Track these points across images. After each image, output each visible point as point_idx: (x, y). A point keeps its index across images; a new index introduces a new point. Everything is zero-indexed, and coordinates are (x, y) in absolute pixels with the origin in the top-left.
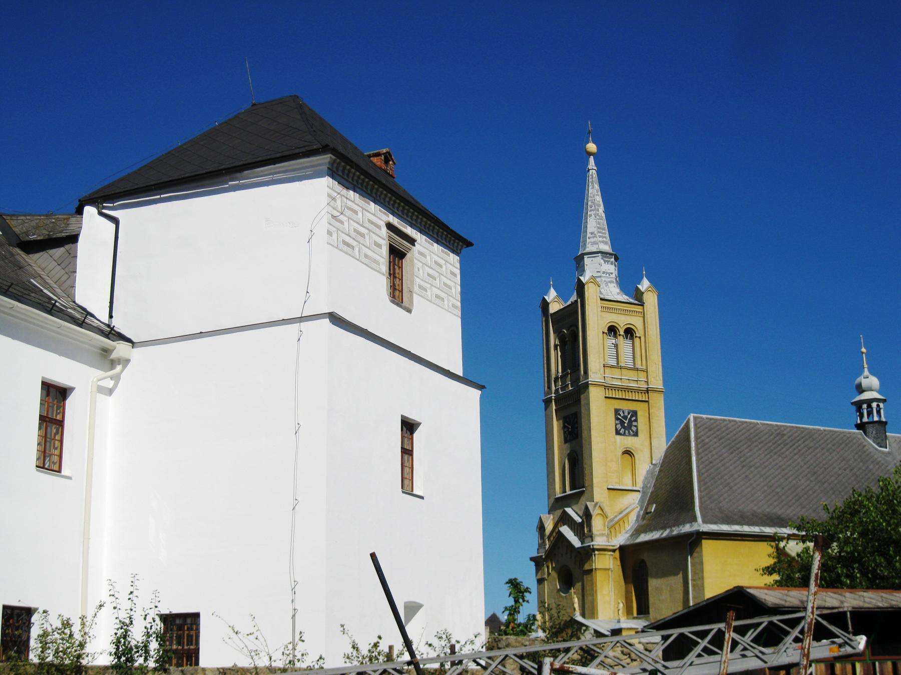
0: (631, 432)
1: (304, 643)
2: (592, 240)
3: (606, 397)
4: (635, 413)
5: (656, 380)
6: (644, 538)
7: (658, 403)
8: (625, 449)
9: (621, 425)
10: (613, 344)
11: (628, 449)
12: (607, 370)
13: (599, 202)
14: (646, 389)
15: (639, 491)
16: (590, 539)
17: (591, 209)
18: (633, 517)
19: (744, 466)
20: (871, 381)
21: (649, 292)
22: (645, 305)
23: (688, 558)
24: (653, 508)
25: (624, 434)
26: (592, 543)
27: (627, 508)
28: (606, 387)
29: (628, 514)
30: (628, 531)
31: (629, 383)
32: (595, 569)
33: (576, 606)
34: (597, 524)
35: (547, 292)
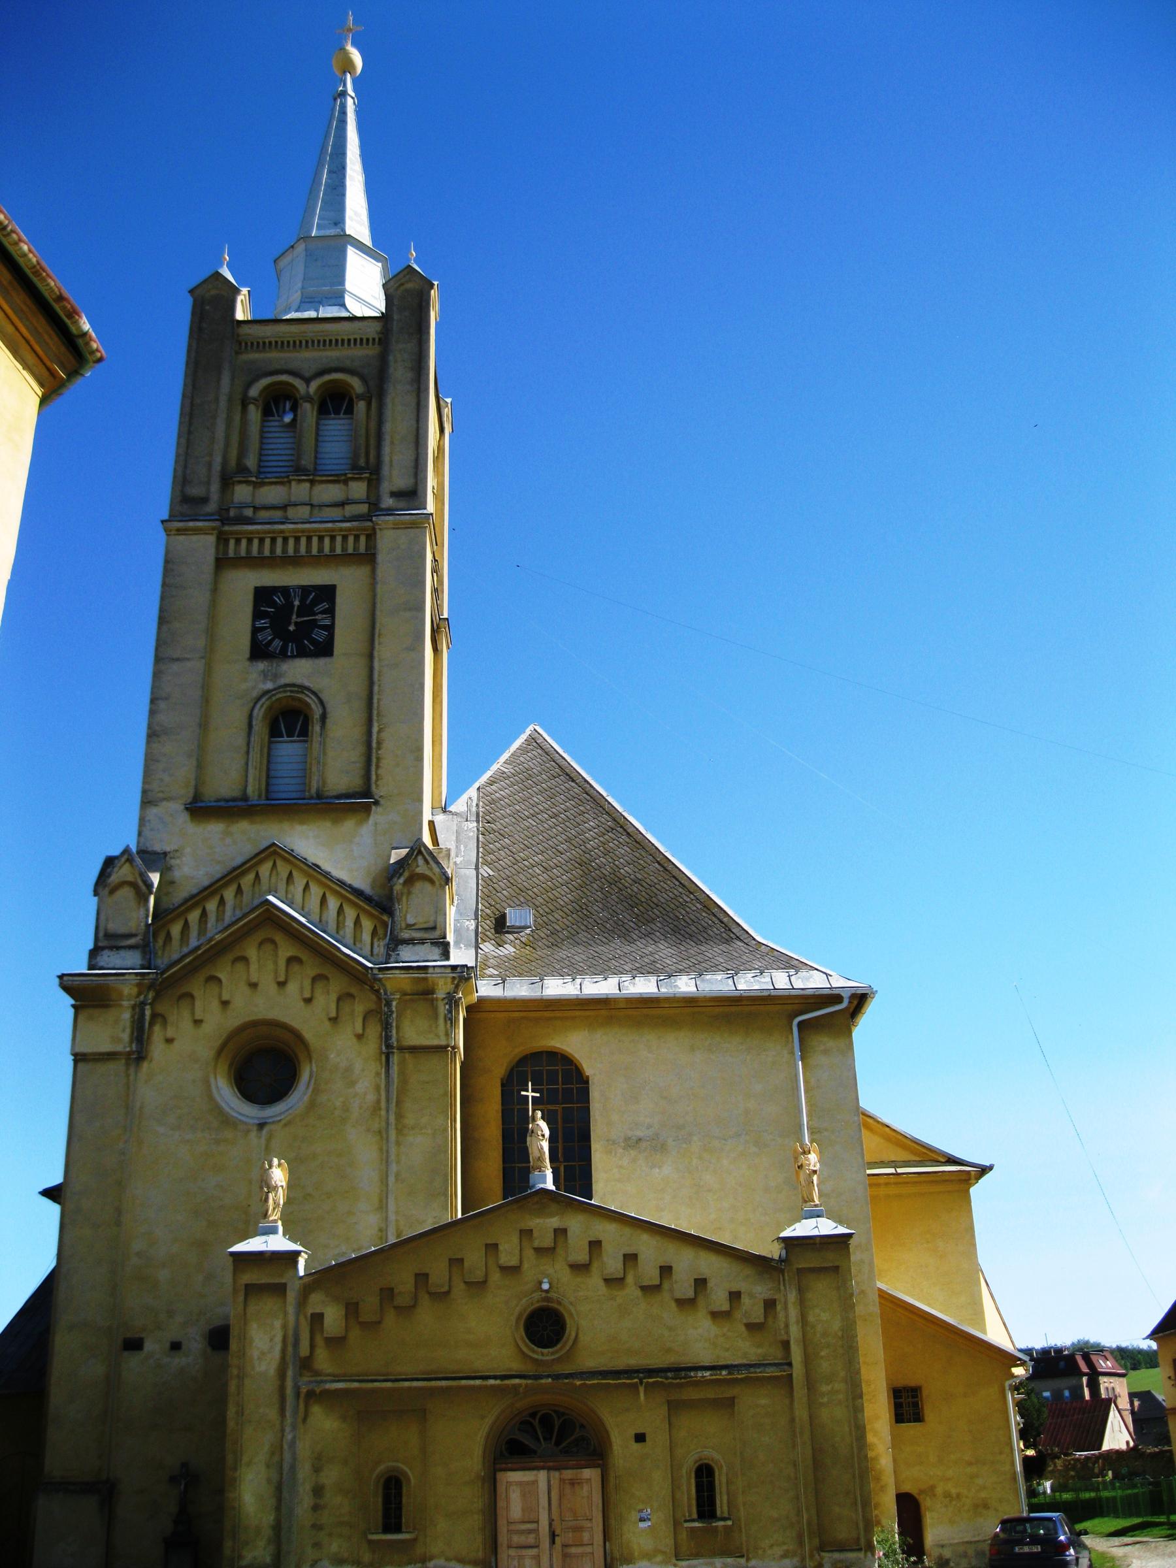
6: (556, 987)
16: (436, 952)
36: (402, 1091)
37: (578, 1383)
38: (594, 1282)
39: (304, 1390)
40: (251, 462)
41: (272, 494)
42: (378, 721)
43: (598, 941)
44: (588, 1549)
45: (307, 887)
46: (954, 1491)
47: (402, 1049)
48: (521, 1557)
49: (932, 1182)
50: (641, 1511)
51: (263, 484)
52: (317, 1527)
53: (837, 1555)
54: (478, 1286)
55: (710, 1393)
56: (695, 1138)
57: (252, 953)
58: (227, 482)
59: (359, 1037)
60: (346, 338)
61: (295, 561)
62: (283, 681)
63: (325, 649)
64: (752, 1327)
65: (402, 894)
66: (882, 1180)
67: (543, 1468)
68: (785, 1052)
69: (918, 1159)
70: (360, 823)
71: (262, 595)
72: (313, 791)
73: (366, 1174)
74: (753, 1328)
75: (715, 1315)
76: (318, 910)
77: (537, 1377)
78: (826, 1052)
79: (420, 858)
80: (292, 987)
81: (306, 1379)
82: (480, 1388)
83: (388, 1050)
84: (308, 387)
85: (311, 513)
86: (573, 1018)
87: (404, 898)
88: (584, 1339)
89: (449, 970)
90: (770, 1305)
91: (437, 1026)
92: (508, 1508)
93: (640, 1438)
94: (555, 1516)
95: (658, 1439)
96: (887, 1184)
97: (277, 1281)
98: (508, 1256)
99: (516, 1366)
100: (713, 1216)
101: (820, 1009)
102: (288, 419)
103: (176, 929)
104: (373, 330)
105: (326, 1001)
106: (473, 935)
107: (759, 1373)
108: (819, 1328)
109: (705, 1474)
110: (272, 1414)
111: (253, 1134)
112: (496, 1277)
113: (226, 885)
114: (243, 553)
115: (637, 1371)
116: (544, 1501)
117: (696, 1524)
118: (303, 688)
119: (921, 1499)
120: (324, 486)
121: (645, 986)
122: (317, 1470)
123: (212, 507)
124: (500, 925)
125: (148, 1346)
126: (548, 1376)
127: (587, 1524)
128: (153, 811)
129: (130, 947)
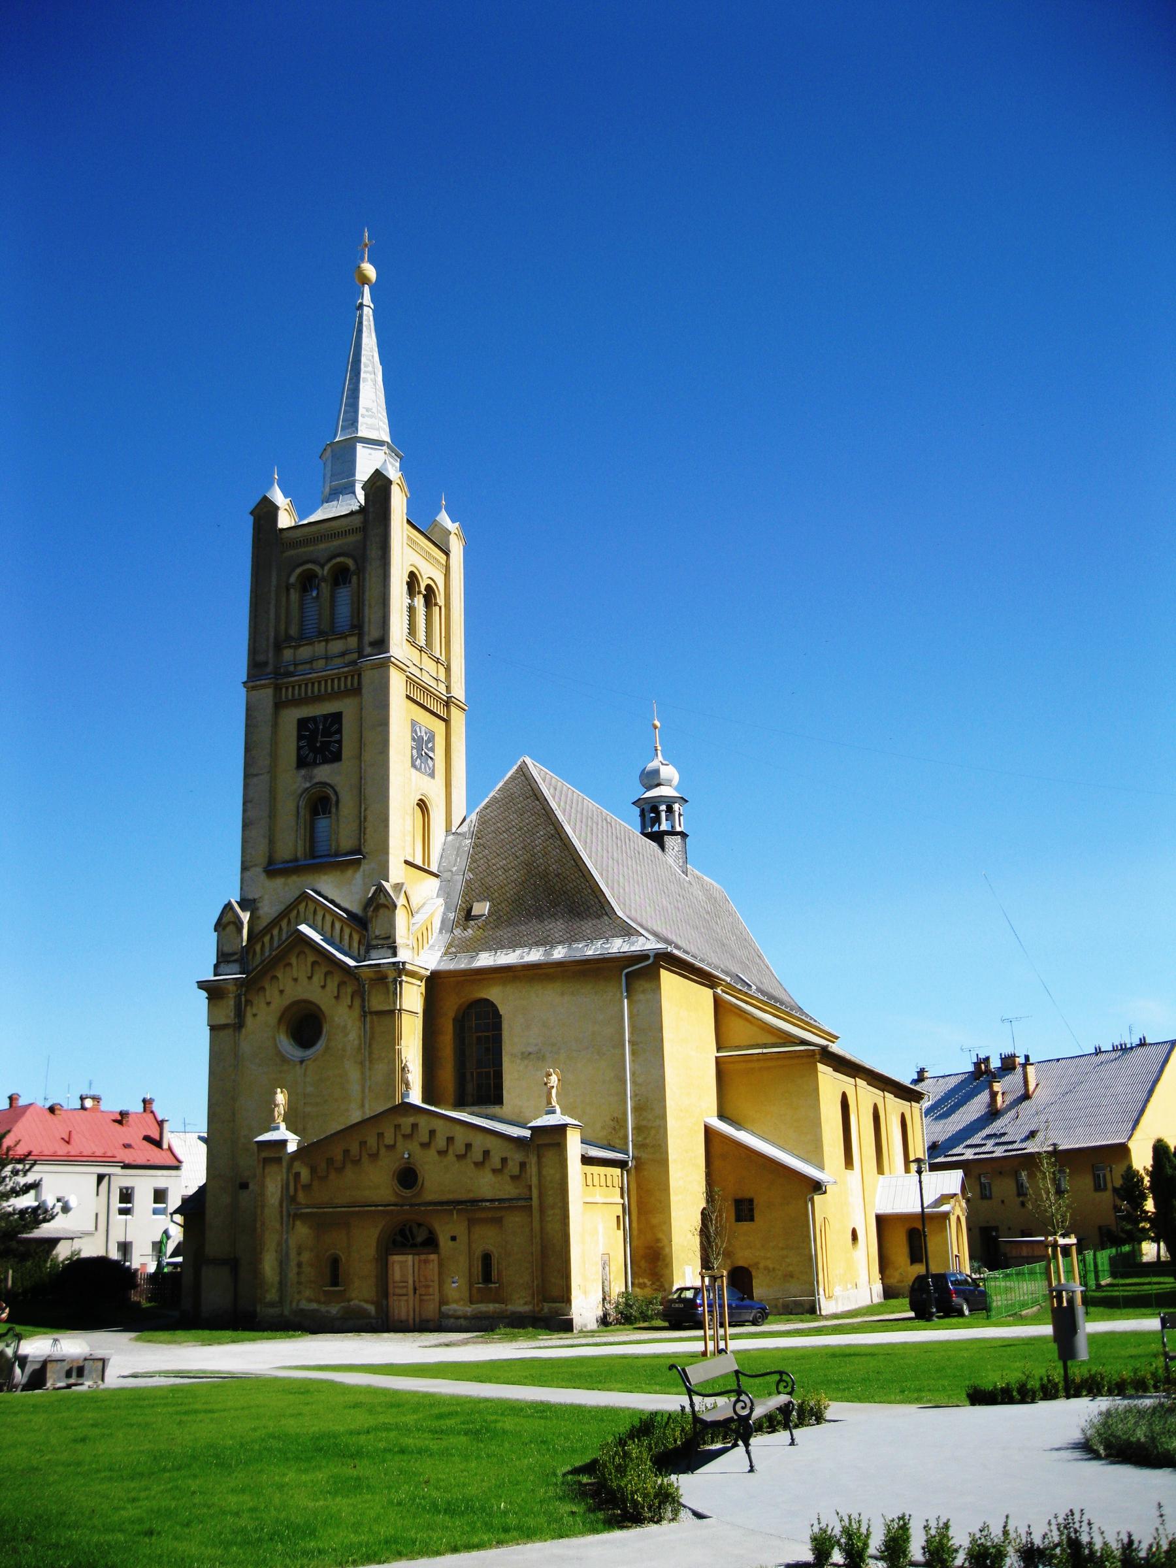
6: (485, 960)
11: (423, 798)
14: (445, 698)
16: (390, 952)
20: (668, 772)
22: (451, 555)
24: (482, 908)
36: (372, 1038)
37: (423, 1208)
38: (432, 1153)
39: (292, 1213)
40: (293, 631)
41: (305, 652)
42: (365, 803)
43: (522, 922)
44: (432, 1297)
45: (324, 916)
46: (771, 1266)
47: (371, 1013)
48: (400, 1300)
50: (453, 1278)
51: (300, 646)
52: (299, 1283)
53: (551, 1304)
54: (374, 1157)
55: (490, 1215)
56: (563, 1051)
57: (294, 961)
58: (278, 648)
59: (350, 1007)
60: (340, 531)
61: (318, 699)
63: (337, 757)
64: (514, 1178)
65: (372, 918)
66: (755, 1058)
67: (411, 1254)
68: (618, 992)
70: (355, 872)
71: (302, 723)
72: (333, 851)
73: (355, 1088)
74: (514, 1178)
75: (494, 1171)
76: (330, 930)
77: (402, 1206)
78: (643, 992)
79: (381, 894)
80: (315, 978)
81: (293, 1207)
82: (375, 1211)
83: (365, 1013)
84: (323, 570)
85: (326, 663)
86: (493, 978)
87: (374, 920)
88: (427, 1184)
89: (391, 965)
90: (523, 1165)
91: (389, 998)
92: (393, 1275)
93: (454, 1238)
94: (416, 1279)
95: (463, 1238)
97: (277, 1156)
98: (389, 1139)
99: (393, 1199)
100: (571, 1100)
102: (314, 594)
103: (258, 948)
105: (332, 986)
106: (451, 922)
107: (515, 1203)
108: (548, 1178)
109: (487, 1258)
110: (278, 1226)
111: (298, 1067)
112: (383, 1151)
113: (282, 919)
114: (290, 697)
115: (453, 1202)
116: (411, 1271)
117: (480, 1285)
118: (325, 784)
119: (750, 1269)
120: (334, 642)
121: (535, 956)
122: (299, 1254)
123: (270, 668)
124: (468, 916)
125: (251, 1186)
126: (407, 1205)
127: (431, 1284)
128: (248, 874)
129: (235, 961)
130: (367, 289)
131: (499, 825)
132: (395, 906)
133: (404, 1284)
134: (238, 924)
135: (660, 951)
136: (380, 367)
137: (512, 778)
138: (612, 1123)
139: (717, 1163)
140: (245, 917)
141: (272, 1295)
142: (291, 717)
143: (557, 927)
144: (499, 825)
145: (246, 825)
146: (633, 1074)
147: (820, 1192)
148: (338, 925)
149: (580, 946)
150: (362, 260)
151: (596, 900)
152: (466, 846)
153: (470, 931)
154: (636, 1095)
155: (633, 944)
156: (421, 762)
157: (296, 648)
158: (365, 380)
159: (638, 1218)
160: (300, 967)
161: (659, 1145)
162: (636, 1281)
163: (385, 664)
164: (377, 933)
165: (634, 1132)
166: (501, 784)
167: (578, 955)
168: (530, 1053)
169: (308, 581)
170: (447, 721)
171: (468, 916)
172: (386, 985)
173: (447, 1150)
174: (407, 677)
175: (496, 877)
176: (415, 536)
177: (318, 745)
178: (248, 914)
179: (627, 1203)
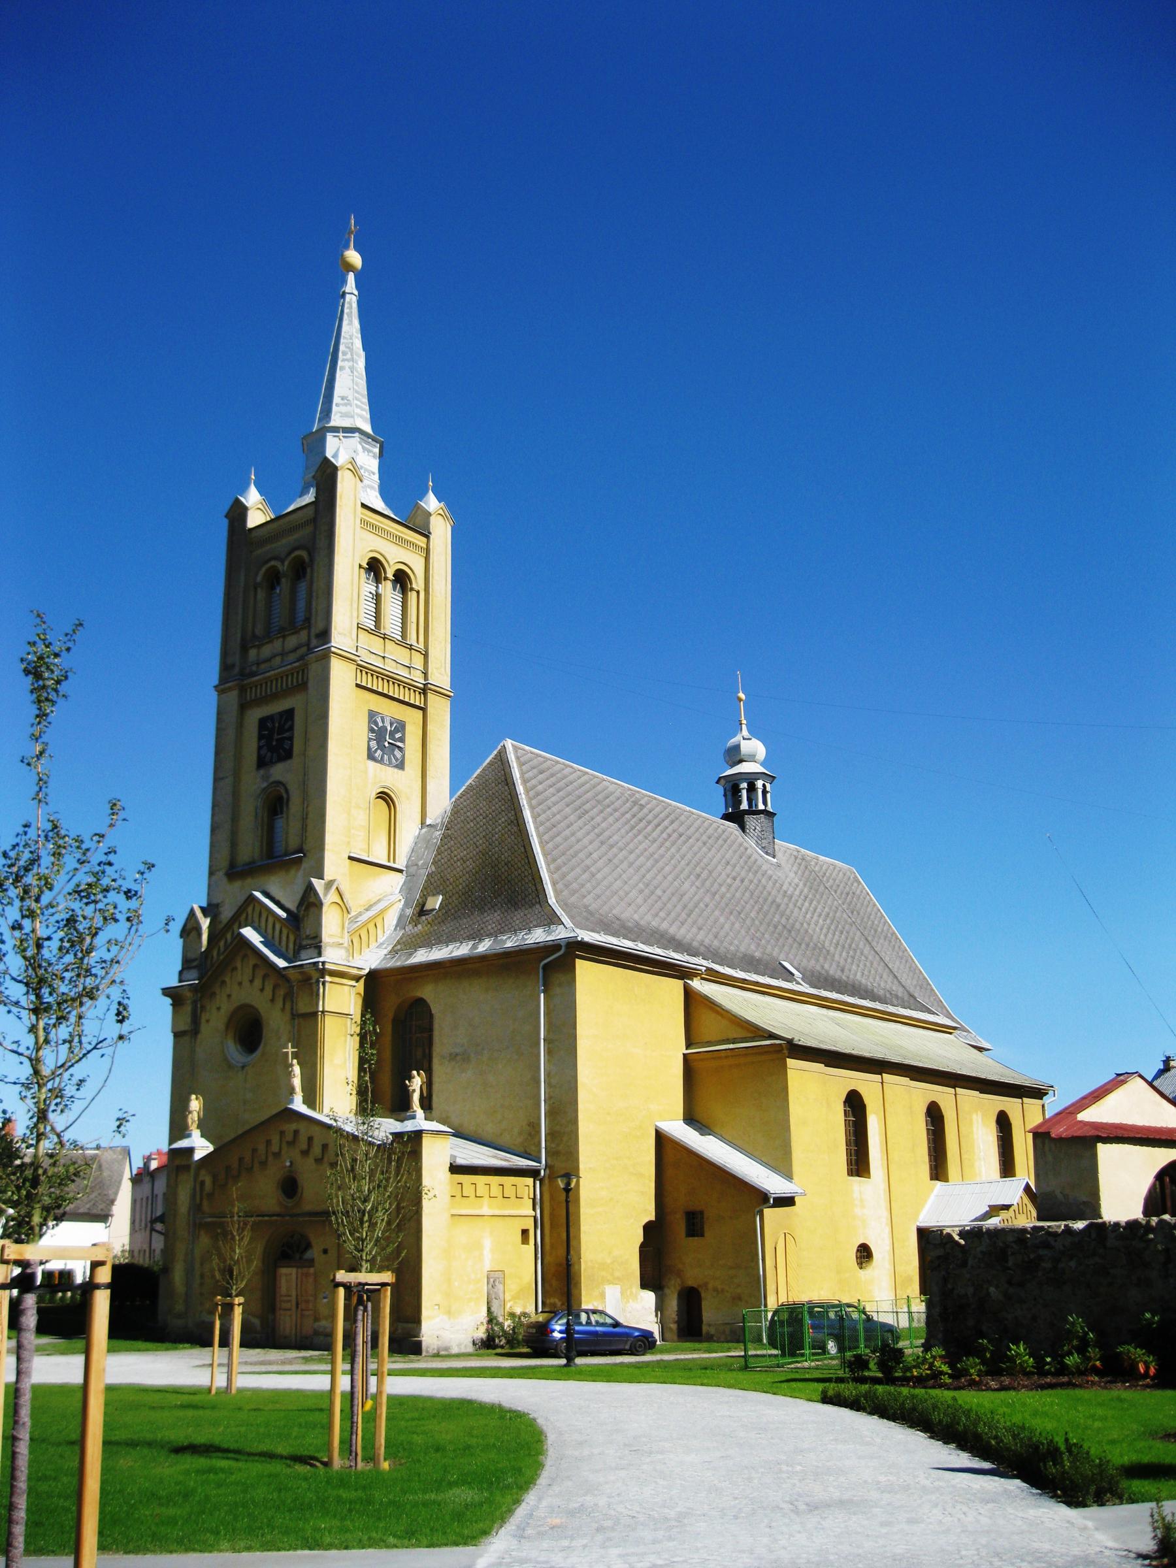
0: (394, 760)
1: (107, 953)
2: (343, 409)
3: (358, 686)
4: (401, 726)
5: (440, 674)
6: (422, 956)
7: (440, 711)
8: (382, 790)
9: (378, 743)
10: (371, 593)
11: (386, 790)
12: (362, 634)
13: (358, 348)
14: (422, 686)
15: (400, 871)
17: (345, 357)
18: (392, 918)
19: (602, 843)
20: (754, 747)
21: (439, 517)
22: (432, 537)
23: (539, 997)
24: (436, 902)
25: (381, 761)
26: (321, 959)
27: (379, 901)
28: (362, 668)
29: (382, 911)
30: (382, 944)
31: (397, 668)
32: (323, 1012)
33: (297, 1082)
34: (331, 924)
35: (244, 489)
37: (301, 1219)
38: (310, 1161)
40: (259, 631)
41: (267, 651)
43: (466, 915)
46: (720, 1287)
49: (756, 1053)
50: (324, 1292)
51: (263, 645)
52: (201, 1294)
56: (485, 1052)
58: (244, 648)
61: (274, 697)
62: (272, 780)
66: (723, 1054)
69: (752, 1035)
70: (298, 870)
71: (263, 722)
78: (560, 985)
83: (295, 1016)
93: (325, 1251)
94: (299, 1293)
96: (727, 1057)
99: (277, 1209)
101: (552, 955)
104: (310, 512)
118: (279, 783)
119: (700, 1289)
121: (462, 950)
122: (202, 1264)
123: (237, 670)
130: (351, 277)
131: (469, 814)
132: (321, 904)
133: (289, 1298)
134: (198, 929)
135: (571, 940)
136: (363, 354)
137: (491, 764)
138: (528, 1128)
139: (669, 1172)
140: (205, 923)
141: (179, 1307)
142: (255, 715)
143: (493, 918)
144: (469, 814)
145: (214, 830)
146: (548, 1075)
147: (768, 1205)
148: (278, 926)
149: (505, 938)
150: (347, 247)
151: (534, 888)
152: (436, 838)
153: (420, 927)
154: (550, 1098)
155: (550, 934)
156: (383, 754)
157: (259, 647)
158: (342, 368)
159: (551, 1232)
160: (243, 971)
161: (571, 1153)
162: (548, 1301)
163: (326, 656)
164: (308, 933)
165: (548, 1138)
166: (479, 771)
167: (498, 948)
168: (457, 1055)
169: (273, 579)
170: (424, 710)
171: (422, 912)
172: (311, 984)
173: (323, 1158)
174: (358, 665)
175: (455, 869)
176: (379, 521)
177: (274, 743)
178: (208, 920)
179: (539, 1216)
